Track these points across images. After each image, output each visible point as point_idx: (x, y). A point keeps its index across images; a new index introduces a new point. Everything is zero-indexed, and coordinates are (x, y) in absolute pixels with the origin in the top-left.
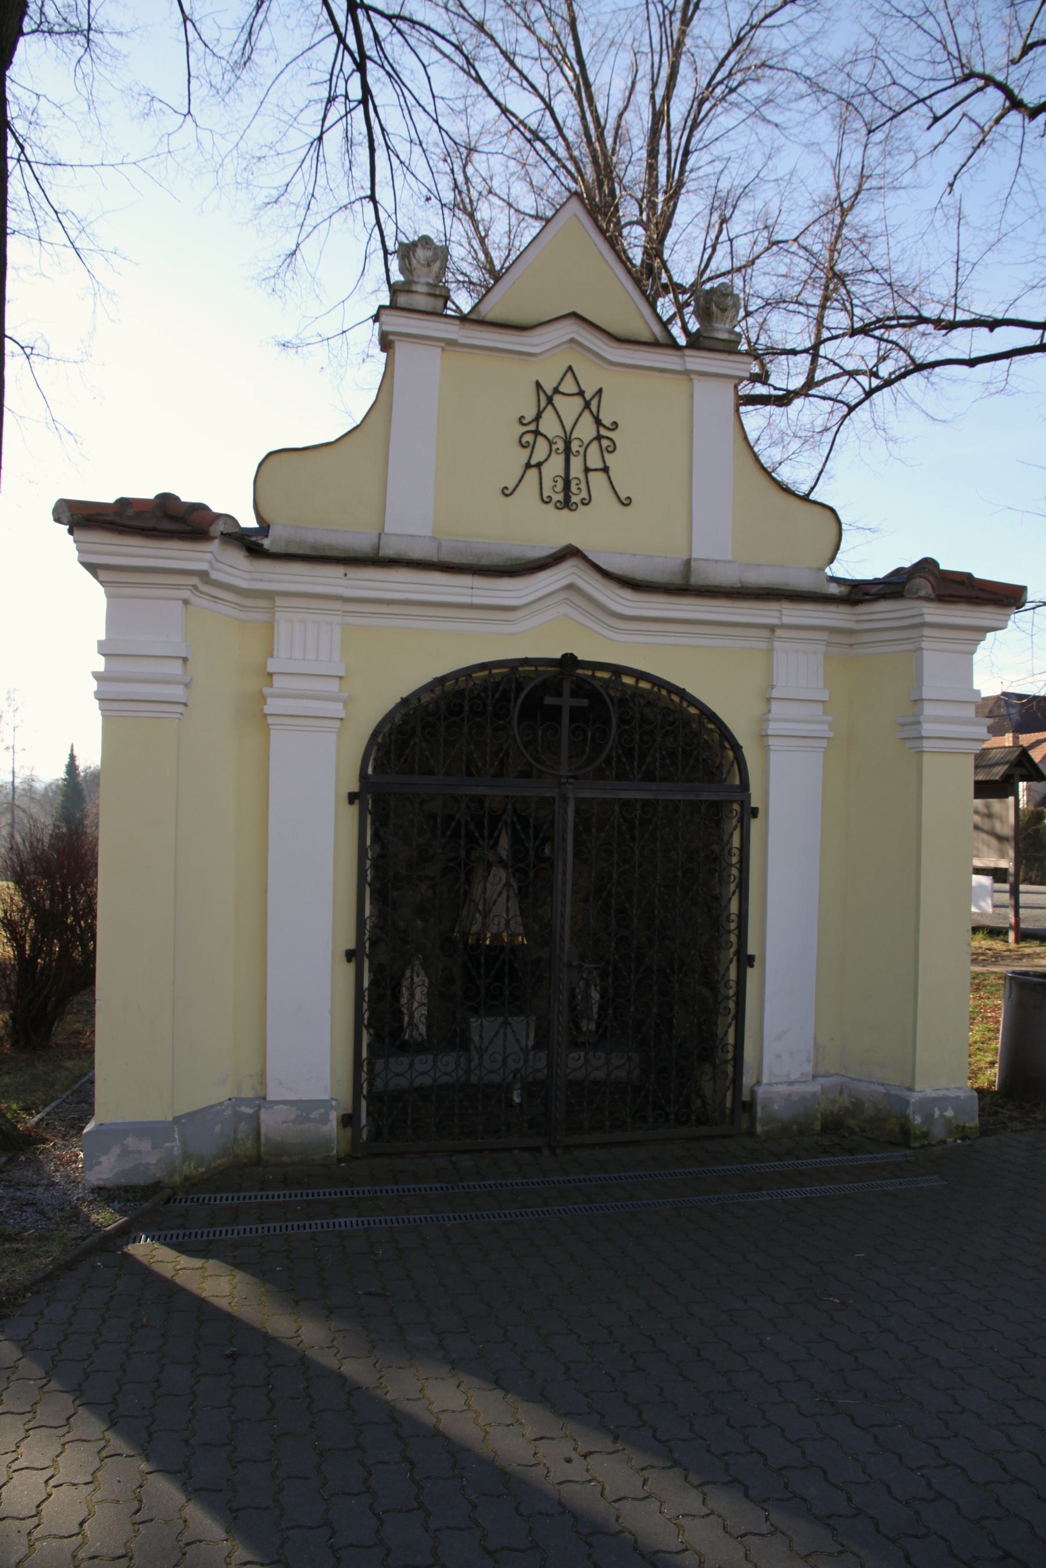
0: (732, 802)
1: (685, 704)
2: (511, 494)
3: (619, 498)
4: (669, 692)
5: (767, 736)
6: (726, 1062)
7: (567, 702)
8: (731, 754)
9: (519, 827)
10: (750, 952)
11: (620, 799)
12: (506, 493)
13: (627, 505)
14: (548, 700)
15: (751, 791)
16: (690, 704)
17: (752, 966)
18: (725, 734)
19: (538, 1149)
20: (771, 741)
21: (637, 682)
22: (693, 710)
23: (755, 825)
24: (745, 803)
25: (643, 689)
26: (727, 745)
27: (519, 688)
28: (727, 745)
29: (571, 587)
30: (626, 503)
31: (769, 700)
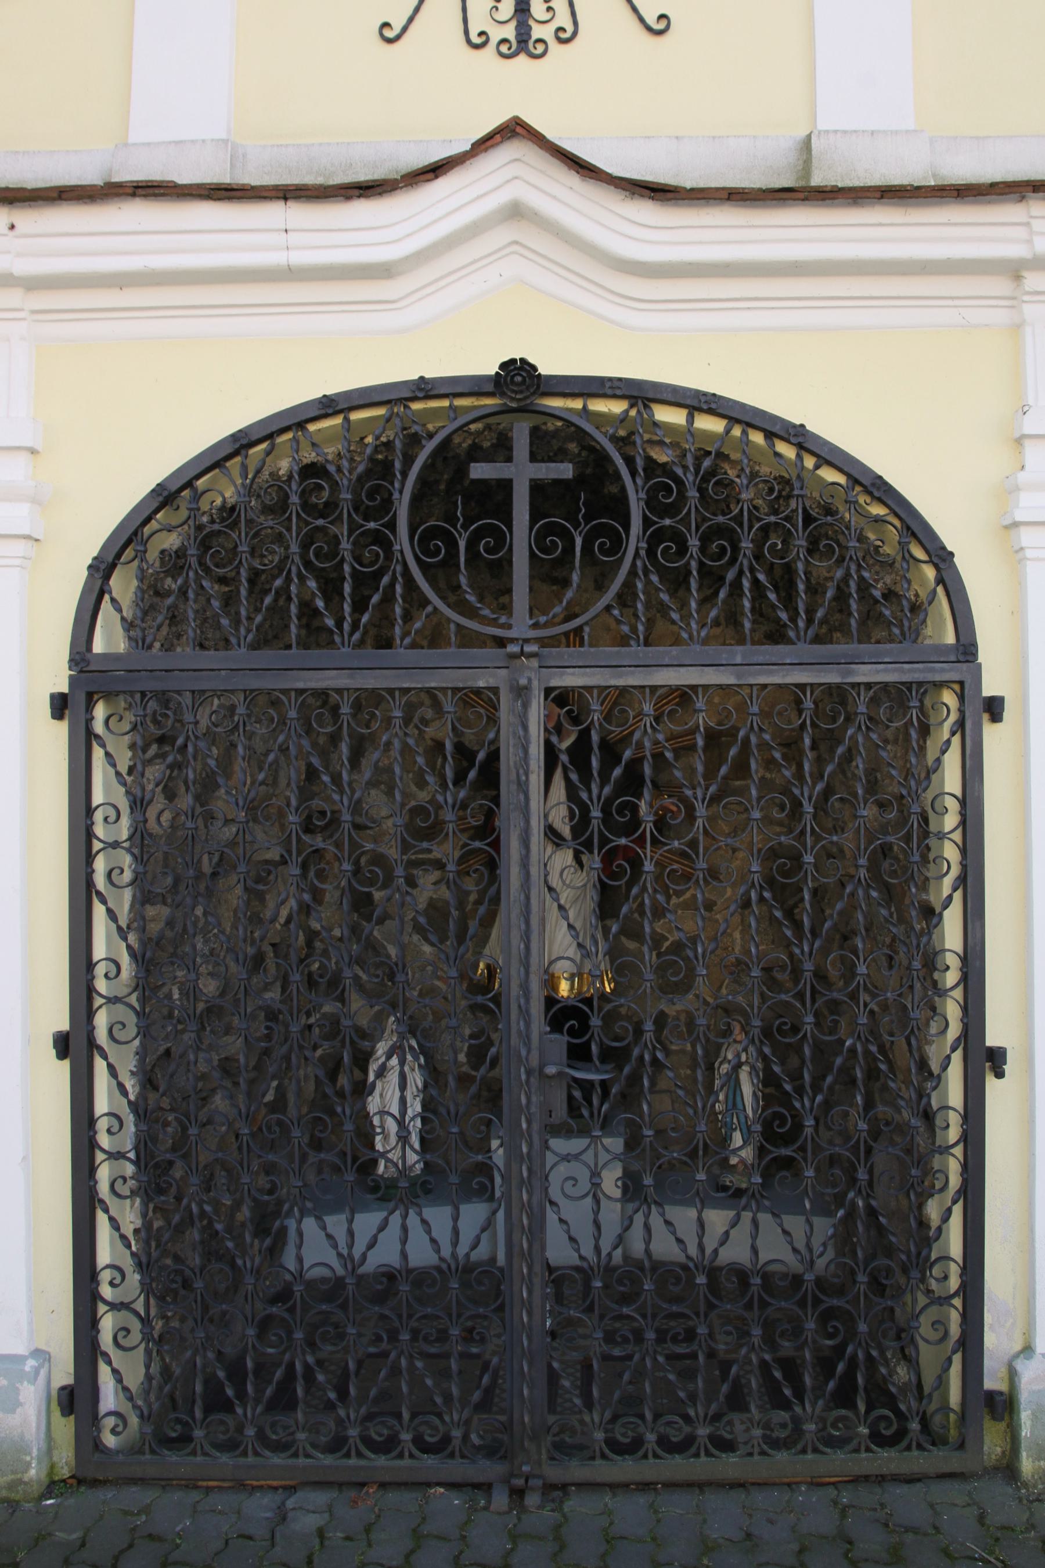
0: (939, 685)
1: (809, 462)
2: (398, 38)
3: (641, 20)
4: (770, 435)
5: (1016, 525)
6: (945, 1300)
7: (522, 472)
8: (930, 573)
9: (778, 1374)
10: (992, 1040)
11: (654, 689)
12: (389, 36)
13: (660, 33)
14: (479, 471)
15: (981, 658)
16: (823, 461)
17: (1000, 1074)
18: (914, 527)
19: (485, 1487)
20: (1027, 537)
21: (691, 419)
22: (829, 475)
23: (995, 739)
24: (966, 688)
25: (707, 435)
26: (919, 553)
27: (414, 441)
28: (919, 553)
29: (516, 212)
30: (659, 28)
31: (1019, 441)
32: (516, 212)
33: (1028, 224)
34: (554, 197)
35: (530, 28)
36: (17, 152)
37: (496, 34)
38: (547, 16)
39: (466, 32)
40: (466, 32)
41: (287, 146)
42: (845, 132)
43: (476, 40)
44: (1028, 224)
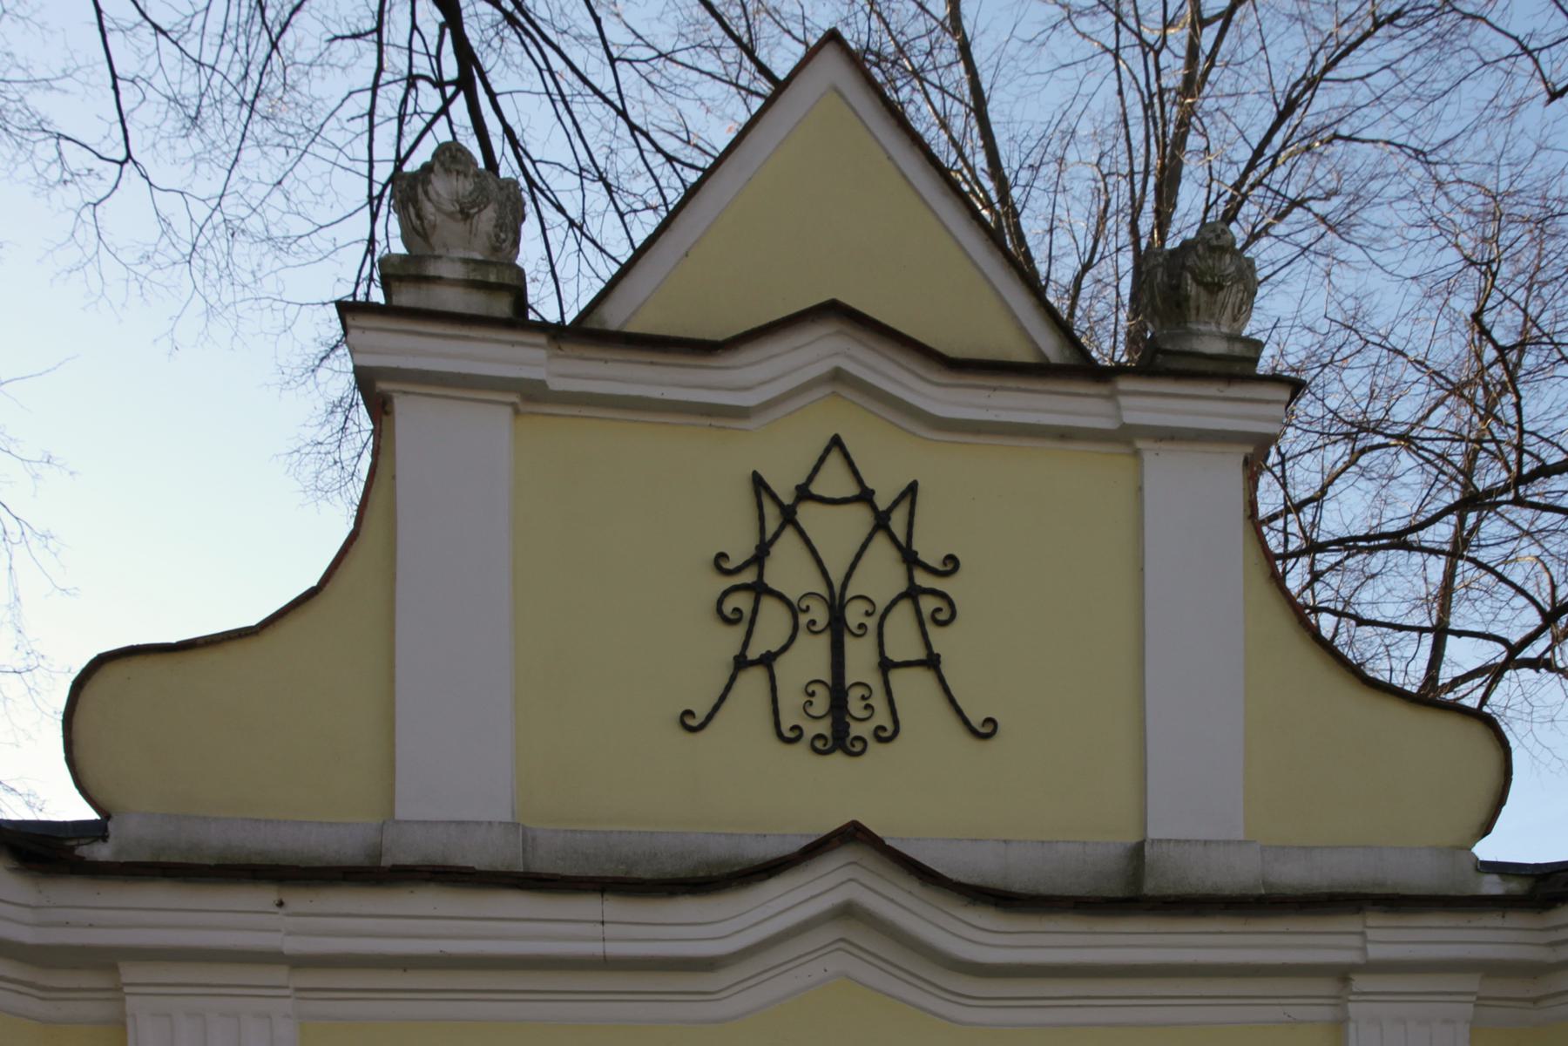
12: (689, 723)
30: (986, 731)
32: (847, 912)
33: (1362, 934)
34: (892, 900)
35: (848, 725)
36: (257, 820)
37: (811, 729)
38: (864, 714)
39: (777, 724)
40: (777, 724)
41: (581, 832)
42: (1178, 841)
43: (788, 734)
44: (1362, 934)
